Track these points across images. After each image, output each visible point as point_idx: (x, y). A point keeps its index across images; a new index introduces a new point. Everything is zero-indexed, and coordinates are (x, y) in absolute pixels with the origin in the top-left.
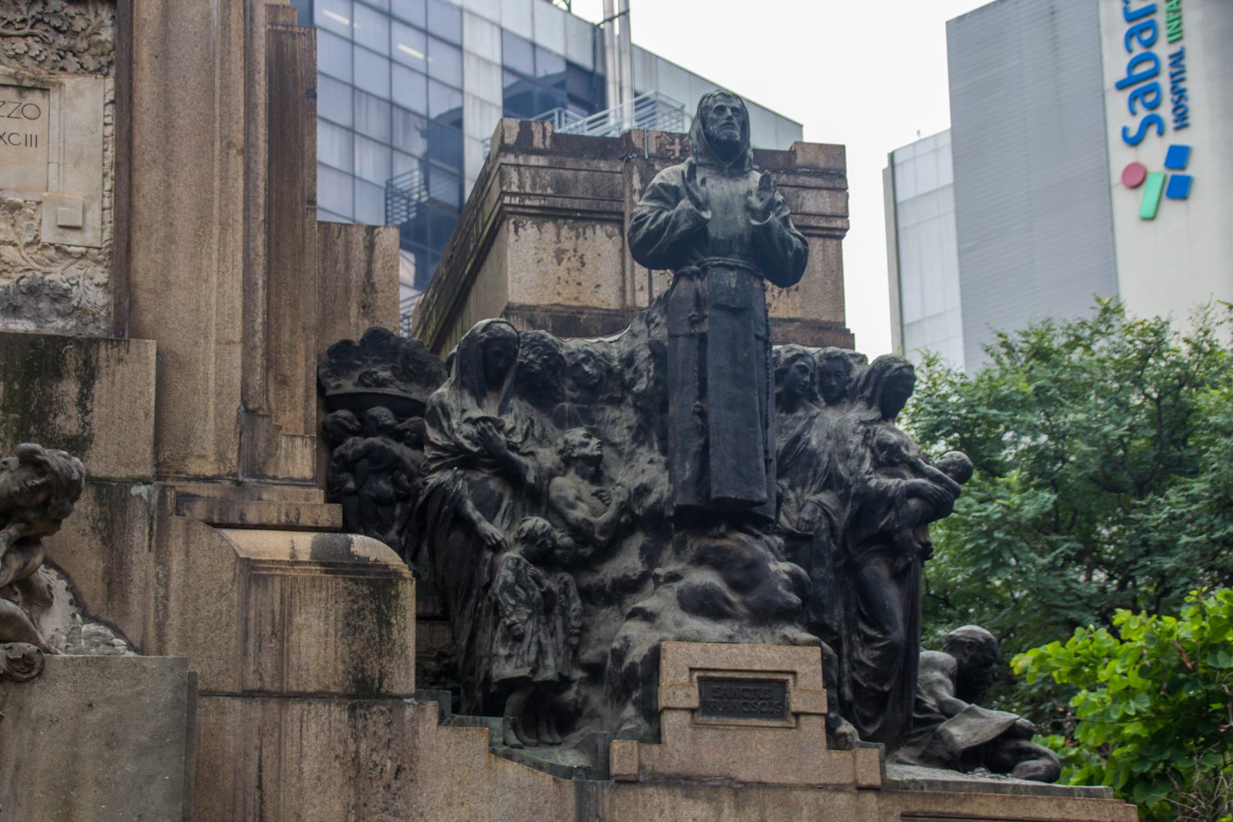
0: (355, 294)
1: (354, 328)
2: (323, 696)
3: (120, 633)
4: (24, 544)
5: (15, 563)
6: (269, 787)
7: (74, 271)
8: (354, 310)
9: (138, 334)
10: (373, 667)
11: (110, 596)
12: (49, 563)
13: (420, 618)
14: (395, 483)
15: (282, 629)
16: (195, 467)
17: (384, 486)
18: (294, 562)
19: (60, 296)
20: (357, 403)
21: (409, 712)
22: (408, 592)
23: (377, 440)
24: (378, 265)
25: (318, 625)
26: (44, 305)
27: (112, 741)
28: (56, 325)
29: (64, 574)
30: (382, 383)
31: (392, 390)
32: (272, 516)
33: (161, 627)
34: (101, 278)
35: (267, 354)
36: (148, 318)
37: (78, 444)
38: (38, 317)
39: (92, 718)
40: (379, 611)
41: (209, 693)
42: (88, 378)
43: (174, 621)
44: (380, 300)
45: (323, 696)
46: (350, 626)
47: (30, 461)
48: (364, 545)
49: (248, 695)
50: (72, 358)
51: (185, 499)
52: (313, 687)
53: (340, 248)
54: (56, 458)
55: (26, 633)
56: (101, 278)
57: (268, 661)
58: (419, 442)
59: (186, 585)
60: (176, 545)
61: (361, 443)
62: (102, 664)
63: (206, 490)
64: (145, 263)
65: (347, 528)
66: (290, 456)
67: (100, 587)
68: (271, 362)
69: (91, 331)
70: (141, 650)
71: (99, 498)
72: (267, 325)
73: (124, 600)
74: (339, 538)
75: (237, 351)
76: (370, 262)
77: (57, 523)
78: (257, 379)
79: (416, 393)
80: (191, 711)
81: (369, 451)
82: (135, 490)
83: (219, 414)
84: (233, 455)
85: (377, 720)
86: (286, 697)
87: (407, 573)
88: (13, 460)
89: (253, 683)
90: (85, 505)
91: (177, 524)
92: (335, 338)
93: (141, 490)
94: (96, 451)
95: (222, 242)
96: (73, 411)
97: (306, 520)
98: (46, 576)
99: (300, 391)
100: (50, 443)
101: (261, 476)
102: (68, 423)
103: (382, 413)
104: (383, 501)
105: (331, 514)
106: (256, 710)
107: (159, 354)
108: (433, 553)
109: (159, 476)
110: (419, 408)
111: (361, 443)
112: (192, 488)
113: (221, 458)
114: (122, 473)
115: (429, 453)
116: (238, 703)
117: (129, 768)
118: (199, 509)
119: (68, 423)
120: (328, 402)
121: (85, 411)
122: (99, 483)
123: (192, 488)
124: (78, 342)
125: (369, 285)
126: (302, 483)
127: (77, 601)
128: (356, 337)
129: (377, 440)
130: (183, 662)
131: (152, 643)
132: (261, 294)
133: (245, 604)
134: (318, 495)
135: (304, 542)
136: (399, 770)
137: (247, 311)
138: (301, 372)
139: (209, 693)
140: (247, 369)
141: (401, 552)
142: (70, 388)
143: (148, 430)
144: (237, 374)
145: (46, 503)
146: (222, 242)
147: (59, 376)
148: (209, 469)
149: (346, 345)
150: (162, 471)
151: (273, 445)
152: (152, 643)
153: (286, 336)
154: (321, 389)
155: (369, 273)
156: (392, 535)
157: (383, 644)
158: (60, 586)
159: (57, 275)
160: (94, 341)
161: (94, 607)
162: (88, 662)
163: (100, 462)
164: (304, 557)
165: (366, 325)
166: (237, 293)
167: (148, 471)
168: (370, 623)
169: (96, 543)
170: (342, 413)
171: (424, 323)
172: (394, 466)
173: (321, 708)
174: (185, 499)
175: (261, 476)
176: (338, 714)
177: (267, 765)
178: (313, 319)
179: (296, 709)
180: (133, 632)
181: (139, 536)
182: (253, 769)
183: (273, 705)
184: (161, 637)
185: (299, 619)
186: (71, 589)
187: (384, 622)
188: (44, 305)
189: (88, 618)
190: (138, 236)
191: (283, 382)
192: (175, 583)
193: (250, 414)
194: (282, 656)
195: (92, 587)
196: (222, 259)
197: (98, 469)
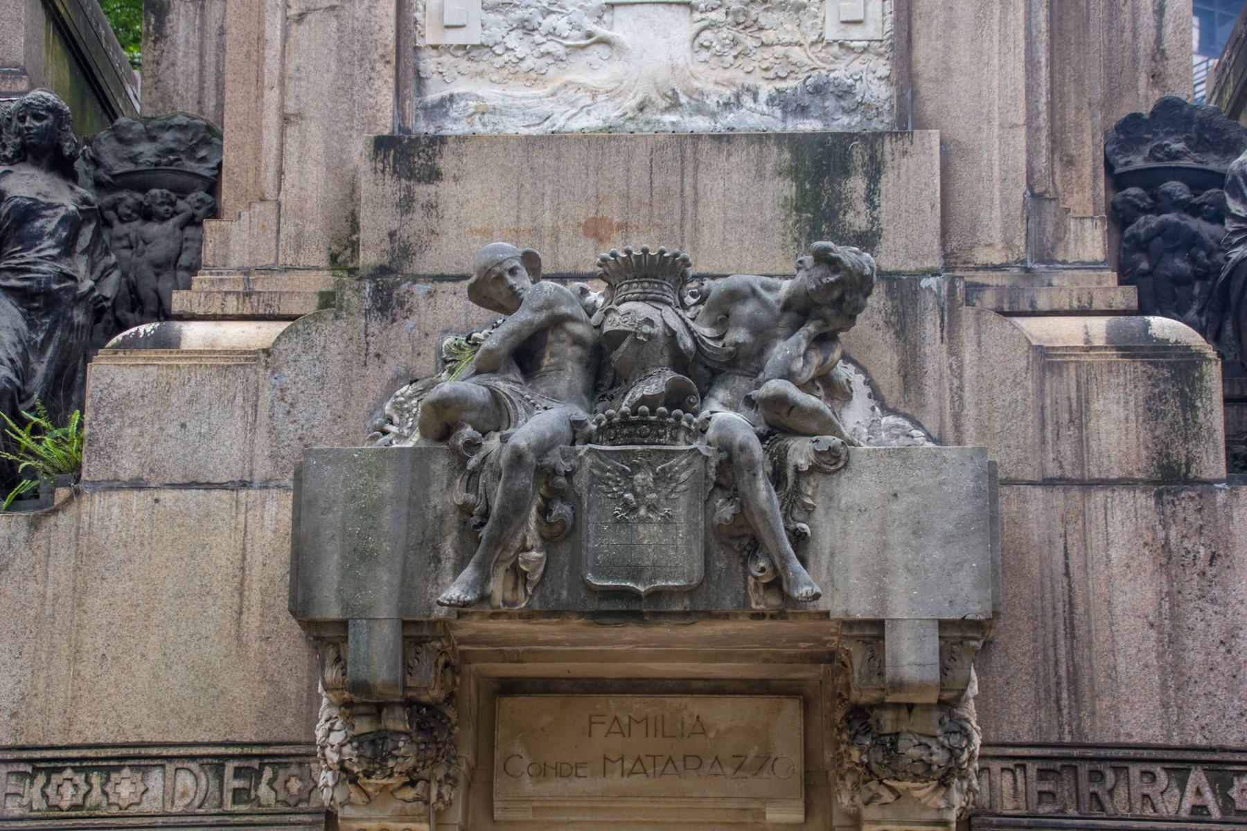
0: (1144, 63)
1: (1143, 100)
2: (1127, 483)
3: (918, 425)
4: (822, 340)
5: (816, 359)
6: (1076, 574)
7: (857, 66)
8: (1143, 80)
9: (921, 125)
10: (1179, 452)
11: (906, 389)
12: (846, 358)
13: (1228, 400)
14: (1193, 260)
15: (1080, 416)
16: (982, 256)
17: (1180, 264)
18: (1089, 348)
19: (845, 92)
20: (1147, 179)
21: (1221, 497)
22: (1213, 374)
23: (1172, 217)
24: (1168, 30)
25: (1118, 411)
26: (830, 103)
27: (918, 530)
28: (842, 123)
29: (861, 369)
30: (1176, 156)
31: (1186, 163)
32: (1063, 302)
33: (957, 417)
34: (884, 71)
35: (1052, 135)
36: (930, 108)
37: (867, 240)
38: (825, 116)
39: (898, 507)
40: (1182, 394)
41: (1009, 482)
42: (874, 173)
43: (970, 412)
44: (1171, 67)
45: (1127, 483)
46: (1152, 411)
47: (823, 258)
48: (1162, 326)
49: (1049, 483)
50: (859, 155)
51: (974, 289)
52: (1115, 474)
53: (1126, 15)
54: (848, 254)
55: (829, 427)
56: (884, 71)
57: (1067, 449)
58: (1219, 215)
59: (980, 375)
60: (967, 334)
61: (1154, 221)
62: (903, 455)
63: (994, 279)
64: (926, 51)
65: (1143, 310)
66: (1080, 239)
67: (896, 380)
68: (1057, 143)
69: (876, 125)
70: (939, 441)
71: (890, 292)
72: (1051, 104)
73: (920, 392)
74: (1135, 321)
75: (1022, 133)
76: (1159, 27)
77: (852, 319)
78: (1042, 162)
79: (1213, 163)
80: (993, 500)
81: (1163, 229)
82: (925, 283)
83: (1005, 201)
84: (1020, 242)
85: (1186, 506)
86: (1088, 485)
87: (1211, 353)
88: (808, 259)
89: (1053, 471)
90: (877, 300)
91: (967, 314)
92: (1124, 112)
93: (930, 282)
94: (884, 246)
95: (1003, 21)
96: (862, 207)
97: (1098, 304)
98: (844, 371)
99: (1087, 171)
100: (841, 240)
101: (1050, 262)
102: (857, 220)
103: (1176, 187)
104: (1179, 280)
105: (1126, 296)
106: (1058, 497)
107: (945, 153)
108: (1238, 332)
109: (947, 267)
110: (1217, 179)
111: (1154, 221)
112: (980, 277)
113: (1008, 245)
114: (912, 266)
115: (1230, 226)
116: (1039, 492)
117: (937, 555)
118: (989, 299)
119: (857, 220)
120: (1117, 180)
121: (873, 206)
122: (890, 278)
123: (980, 277)
124: (863, 138)
125: (1159, 53)
126: (1094, 266)
127: (875, 394)
128: (1145, 110)
129: (1172, 217)
130: (982, 451)
131: (950, 433)
132: (1044, 73)
133: (1041, 392)
134: (1111, 278)
135: (1098, 327)
136: (1213, 558)
137: (1030, 91)
138: (1088, 151)
139: (1009, 482)
140: (1031, 152)
141: (1202, 331)
142: (857, 184)
143: (934, 220)
144: (1022, 159)
145: (841, 299)
146: (1003, 21)
147: (847, 173)
148: (996, 258)
149: (1135, 118)
150: (950, 262)
151: (1060, 226)
152: (950, 433)
153: (1071, 114)
154: (1109, 167)
155: (1159, 40)
156: (1192, 314)
157: (1188, 428)
158: (858, 380)
159: (841, 72)
160: (879, 135)
161: (891, 399)
162: (890, 453)
163: (888, 257)
164: (1099, 342)
165: (1156, 95)
166: (1020, 73)
167: (936, 262)
168: (1172, 406)
169: (890, 337)
170: (1132, 191)
171: (1219, 88)
172: (1191, 242)
173: (1126, 495)
174: (974, 289)
175: (1050, 262)
176: (1144, 501)
177: (1073, 552)
178: (1098, 94)
179: (1099, 496)
180: (931, 423)
181: (931, 328)
182: (1059, 556)
183: (1075, 493)
184: (958, 427)
185: (1096, 406)
186: (868, 382)
187: (1188, 405)
188: (830, 103)
189: (887, 410)
190: (918, 24)
191: (1070, 162)
192: (969, 373)
193: (1037, 199)
194: (1081, 443)
195: (889, 380)
196: (1003, 39)
197: (888, 264)
